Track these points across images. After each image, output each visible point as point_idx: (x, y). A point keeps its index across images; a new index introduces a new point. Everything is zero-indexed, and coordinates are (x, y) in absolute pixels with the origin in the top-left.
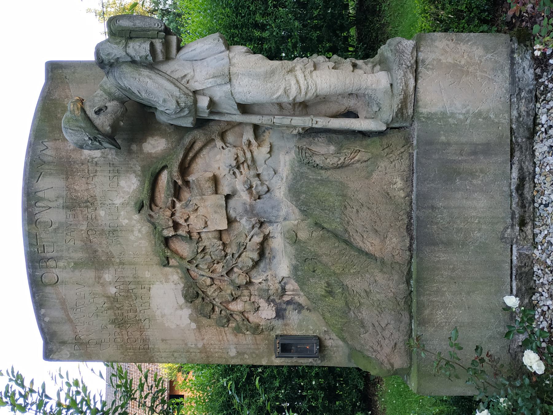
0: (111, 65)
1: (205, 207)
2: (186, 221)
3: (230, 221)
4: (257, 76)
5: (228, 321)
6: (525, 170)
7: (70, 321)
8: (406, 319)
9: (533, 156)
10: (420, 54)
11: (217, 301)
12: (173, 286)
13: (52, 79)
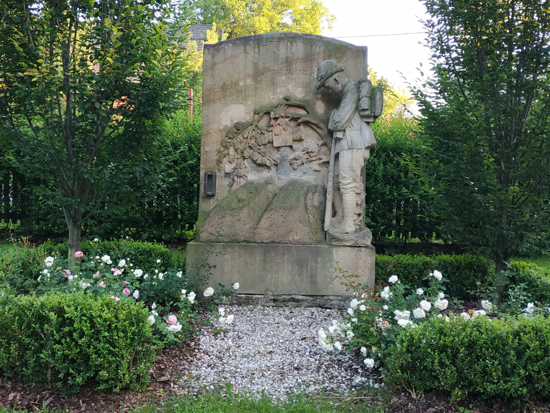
0: (359, 87)
1: (286, 135)
2: (279, 124)
3: (278, 148)
4: (351, 163)
5: (224, 147)
6: (303, 303)
7: (225, 60)
8: (226, 240)
9: (309, 307)
10: (364, 248)
11: (235, 141)
12: (243, 117)
13: (358, 51)
